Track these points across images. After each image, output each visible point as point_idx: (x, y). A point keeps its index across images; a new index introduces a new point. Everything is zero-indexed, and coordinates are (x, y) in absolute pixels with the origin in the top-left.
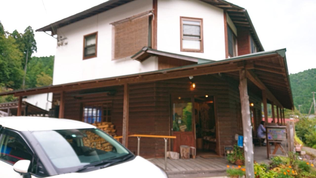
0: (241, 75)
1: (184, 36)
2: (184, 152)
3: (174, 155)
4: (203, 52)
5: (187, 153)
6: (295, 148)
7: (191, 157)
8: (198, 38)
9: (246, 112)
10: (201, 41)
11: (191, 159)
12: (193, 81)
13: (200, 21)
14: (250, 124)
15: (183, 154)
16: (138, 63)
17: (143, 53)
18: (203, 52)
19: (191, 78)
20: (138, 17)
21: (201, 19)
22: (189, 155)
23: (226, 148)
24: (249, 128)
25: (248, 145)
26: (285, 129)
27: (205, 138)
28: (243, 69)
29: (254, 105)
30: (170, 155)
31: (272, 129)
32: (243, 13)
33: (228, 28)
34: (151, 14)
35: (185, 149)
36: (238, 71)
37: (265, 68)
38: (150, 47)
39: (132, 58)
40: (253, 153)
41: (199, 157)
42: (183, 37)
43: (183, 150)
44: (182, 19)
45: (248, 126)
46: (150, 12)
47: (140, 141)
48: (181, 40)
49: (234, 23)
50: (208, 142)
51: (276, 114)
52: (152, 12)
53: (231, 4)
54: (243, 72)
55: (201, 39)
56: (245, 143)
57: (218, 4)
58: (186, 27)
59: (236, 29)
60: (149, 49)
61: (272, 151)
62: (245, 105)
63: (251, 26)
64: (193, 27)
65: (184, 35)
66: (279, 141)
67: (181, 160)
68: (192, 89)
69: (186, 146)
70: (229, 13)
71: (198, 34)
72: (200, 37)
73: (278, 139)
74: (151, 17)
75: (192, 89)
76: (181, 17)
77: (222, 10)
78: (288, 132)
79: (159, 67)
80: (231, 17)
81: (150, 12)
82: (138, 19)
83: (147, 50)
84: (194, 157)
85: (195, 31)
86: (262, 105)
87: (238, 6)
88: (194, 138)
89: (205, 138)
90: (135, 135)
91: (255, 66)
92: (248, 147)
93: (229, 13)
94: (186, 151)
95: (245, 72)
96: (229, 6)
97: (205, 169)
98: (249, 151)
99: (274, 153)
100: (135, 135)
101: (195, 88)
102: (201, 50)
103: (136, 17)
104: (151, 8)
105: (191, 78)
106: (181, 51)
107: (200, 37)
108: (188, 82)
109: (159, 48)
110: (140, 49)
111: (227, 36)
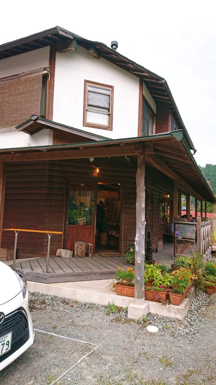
0: (139, 161)
1: (88, 107)
2: (78, 249)
3: (65, 253)
4: (112, 130)
5: (82, 251)
6: (210, 247)
7: (87, 255)
8: (107, 111)
9: (140, 205)
10: (110, 115)
11: (86, 258)
12: (97, 163)
13: (111, 89)
14: (144, 219)
15: (77, 251)
16: (27, 136)
17: (32, 122)
18: (112, 130)
19: (92, 159)
20: (29, 74)
21: (112, 87)
22: (84, 253)
23: (129, 245)
24: (142, 224)
25: (138, 244)
26: (195, 226)
27: (110, 233)
28: (142, 154)
29: (170, 196)
30: (61, 253)
31: (180, 225)
32: (162, 85)
33: (144, 103)
34: (45, 72)
35: (80, 246)
36: (137, 156)
37: (166, 152)
38: (43, 117)
39: (17, 128)
40: (144, 253)
41: (97, 255)
42: (87, 107)
43: (77, 248)
44: (88, 84)
45: (141, 221)
46: (45, 69)
47: (18, 236)
48: (85, 111)
49: (153, 97)
50: (113, 237)
51: (199, 208)
52: (48, 69)
53: (149, 72)
54: (142, 157)
55: (110, 113)
56: (137, 241)
57: (134, 71)
58: (91, 95)
59: (156, 105)
60: (40, 118)
61: (179, 250)
62: (140, 196)
63: (172, 102)
64: (101, 95)
65: (89, 105)
66: (188, 239)
67: (74, 259)
68: (95, 175)
69: (82, 243)
70: (146, 83)
71: (107, 106)
72: (109, 110)
73: (186, 237)
74: (45, 77)
75: (95, 175)
76: (86, 82)
77: (139, 78)
78: (198, 229)
79: (54, 142)
80: (148, 88)
81: (45, 69)
82: (29, 77)
83: (37, 119)
84: (90, 255)
85: (103, 102)
86: (183, 199)
87: (156, 75)
88: (94, 233)
89: (110, 233)
90: (12, 229)
91: (156, 150)
92: (139, 247)
93: (146, 83)
94: (81, 249)
95: (144, 157)
96: (146, 74)
97: (96, 270)
98: (139, 251)
99: (182, 252)
100: (12, 229)
101: (98, 173)
102: (109, 127)
103: (26, 75)
104: (47, 65)
105: (92, 159)
106: (84, 125)
107: (109, 110)
108: (90, 166)
109: (55, 120)
110: (28, 117)
111: (141, 112)
